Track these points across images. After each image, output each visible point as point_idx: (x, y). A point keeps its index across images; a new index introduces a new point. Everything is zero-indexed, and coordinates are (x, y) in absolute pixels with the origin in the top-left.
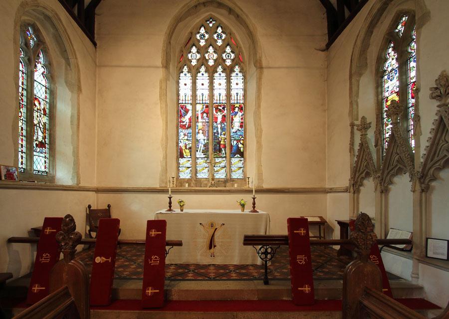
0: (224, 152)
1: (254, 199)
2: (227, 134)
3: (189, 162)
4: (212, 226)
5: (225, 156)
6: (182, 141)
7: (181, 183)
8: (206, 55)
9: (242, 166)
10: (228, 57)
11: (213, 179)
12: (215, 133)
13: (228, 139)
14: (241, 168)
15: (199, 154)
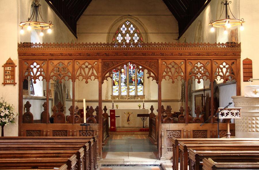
0: (134, 83)
1: (144, 104)
2: (136, 74)
3: (118, 88)
4: (128, 113)
5: (134, 84)
6: (114, 78)
7: (114, 98)
8: (126, 38)
9: (143, 89)
10: (136, 38)
11: (129, 96)
12: (130, 74)
13: (136, 77)
14: (142, 90)
15: (123, 84)
